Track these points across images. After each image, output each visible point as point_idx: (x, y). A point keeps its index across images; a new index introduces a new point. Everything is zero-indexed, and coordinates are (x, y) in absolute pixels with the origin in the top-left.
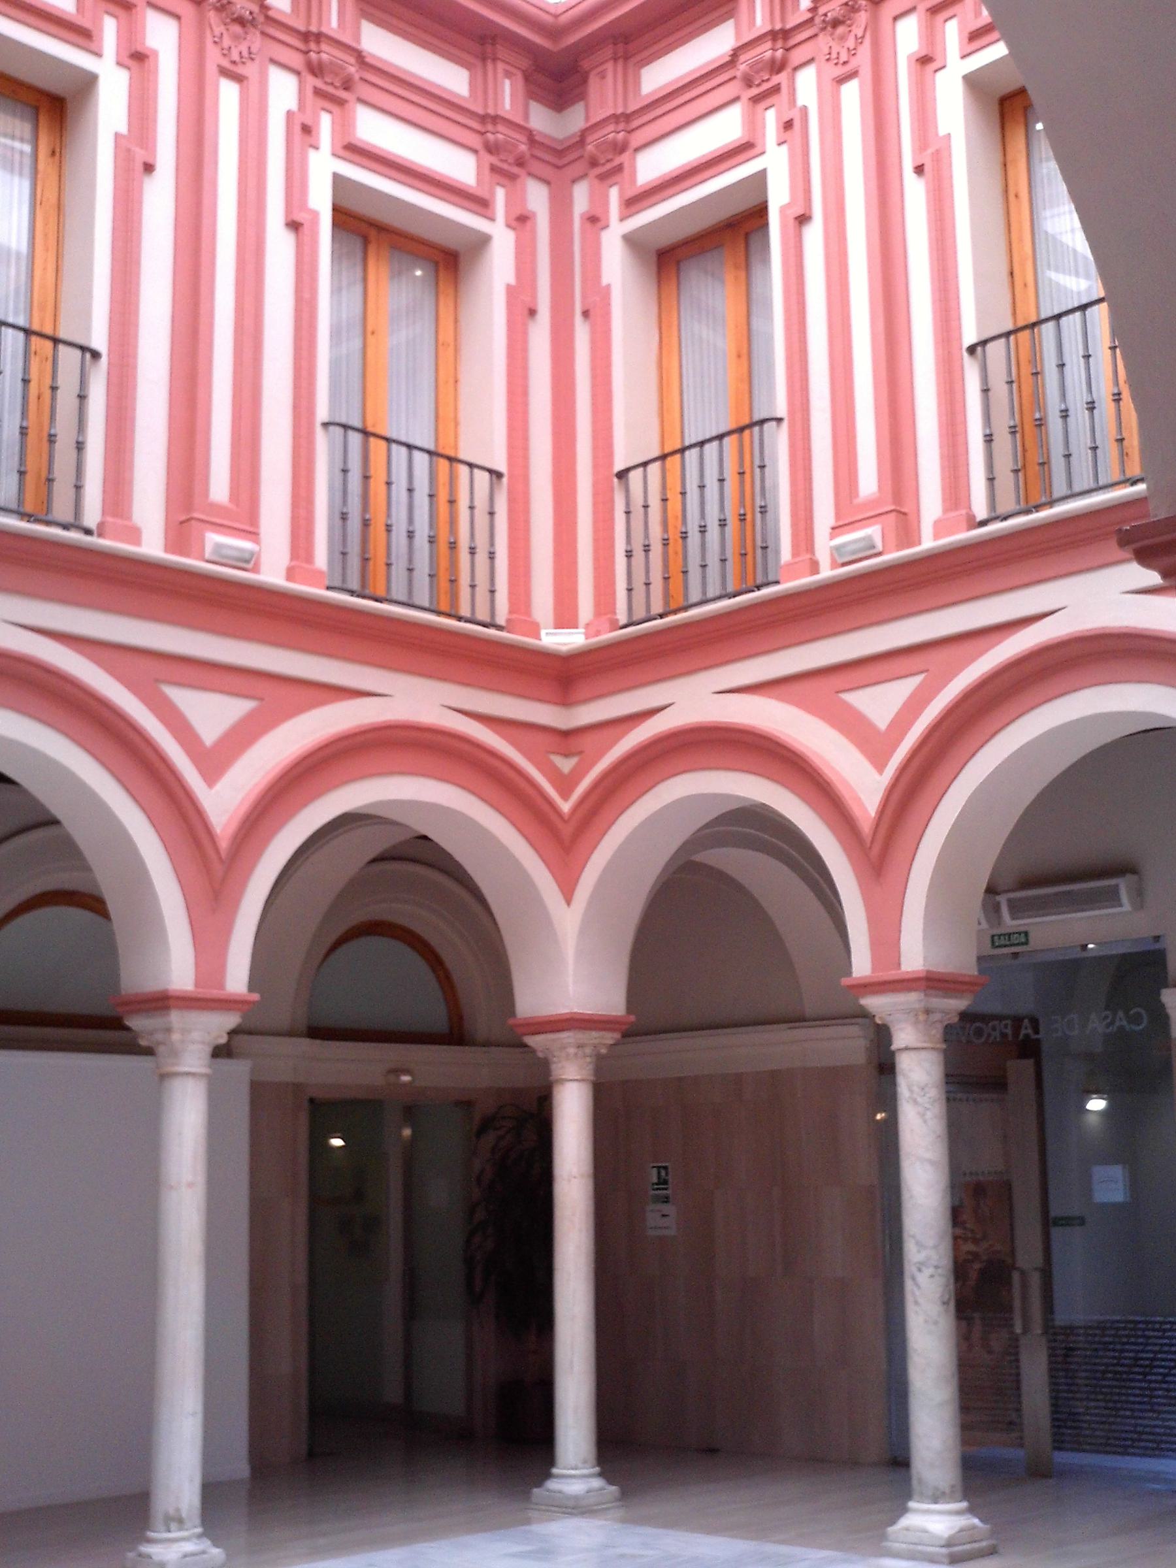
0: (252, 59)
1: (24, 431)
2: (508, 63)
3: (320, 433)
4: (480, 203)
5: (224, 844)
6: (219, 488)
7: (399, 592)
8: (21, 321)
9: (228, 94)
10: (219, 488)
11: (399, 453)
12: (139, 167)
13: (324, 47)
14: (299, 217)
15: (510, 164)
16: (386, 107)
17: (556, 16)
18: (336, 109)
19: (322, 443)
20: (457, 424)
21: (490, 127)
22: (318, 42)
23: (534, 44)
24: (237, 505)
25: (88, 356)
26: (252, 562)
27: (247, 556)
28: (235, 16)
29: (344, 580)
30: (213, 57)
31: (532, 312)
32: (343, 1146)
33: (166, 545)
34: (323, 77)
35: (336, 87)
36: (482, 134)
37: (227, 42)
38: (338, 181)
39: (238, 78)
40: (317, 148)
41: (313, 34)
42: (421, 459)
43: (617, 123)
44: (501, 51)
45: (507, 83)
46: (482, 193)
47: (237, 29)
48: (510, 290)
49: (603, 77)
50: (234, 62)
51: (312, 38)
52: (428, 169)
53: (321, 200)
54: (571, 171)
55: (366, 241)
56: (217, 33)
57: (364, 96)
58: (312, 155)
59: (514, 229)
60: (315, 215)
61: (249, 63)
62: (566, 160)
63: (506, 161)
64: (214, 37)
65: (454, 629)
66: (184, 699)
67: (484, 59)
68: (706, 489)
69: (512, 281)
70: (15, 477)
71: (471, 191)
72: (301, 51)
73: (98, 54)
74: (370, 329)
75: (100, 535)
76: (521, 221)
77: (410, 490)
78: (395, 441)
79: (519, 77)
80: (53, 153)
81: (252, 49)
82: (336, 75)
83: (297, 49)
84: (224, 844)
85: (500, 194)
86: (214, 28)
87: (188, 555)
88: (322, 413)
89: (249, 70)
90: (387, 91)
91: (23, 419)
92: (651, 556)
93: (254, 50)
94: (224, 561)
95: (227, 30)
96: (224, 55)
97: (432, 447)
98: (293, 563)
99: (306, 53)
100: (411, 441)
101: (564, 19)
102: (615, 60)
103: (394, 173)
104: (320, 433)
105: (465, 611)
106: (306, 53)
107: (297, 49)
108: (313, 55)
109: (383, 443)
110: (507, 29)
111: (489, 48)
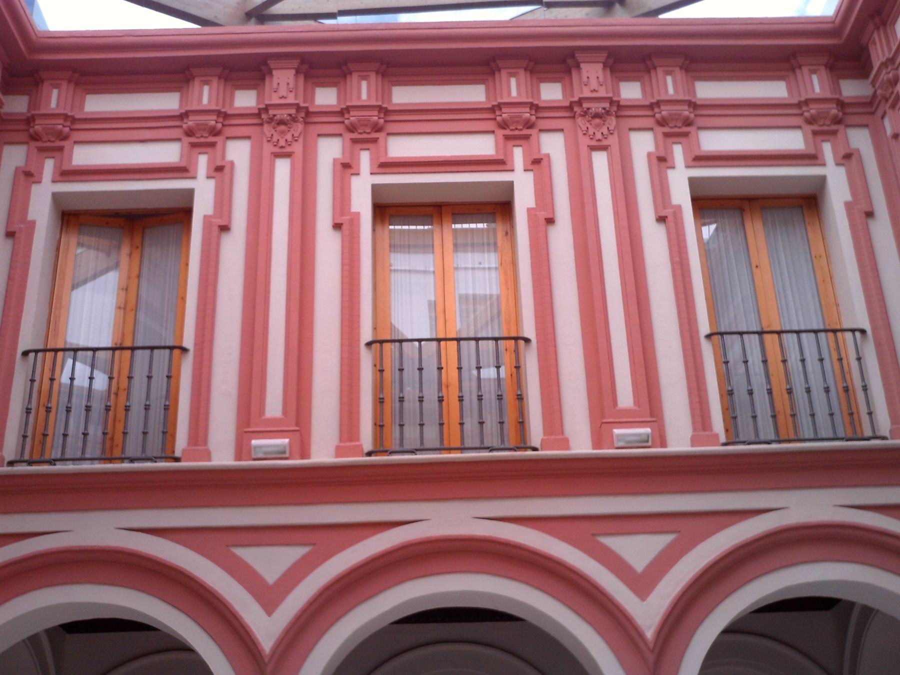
0: (611, 134)
1: (69, 409)
2: (809, 65)
3: (363, 351)
4: (811, 158)
5: (649, 634)
6: (625, 397)
7: (808, 433)
8: (755, 328)
9: (600, 162)
10: (625, 397)
11: (790, 340)
12: (543, 222)
13: (811, 106)
14: (15, 227)
15: (828, 125)
16: (437, 130)
17: (833, 22)
18: (683, 140)
19: (707, 351)
20: (837, 305)
21: (804, 108)
22: (659, 107)
23: (829, 45)
24: (639, 406)
25: (858, 334)
26: (650, 440)
27: (645, 438)
28: (593, 114)
29: (835, 432)
30: (584, 142)
31: (870, 214)
32: (717, 229)
33: (593, 445)
34: (668, 124)
35: (680, 127)
36: (802, 115)
37: (591, 132)
38: (693, 182)
39: (604, 148)
40: (673, 167)
41: (575, 102)
42: (487, 347)
43: (887, 67)
44: (500, 63)
45: (815, 78)
46: (812, 151)
47: (597, 121)
48: (848, 206)
49: (875, 44)
50: (599, 140)
51: (345, 112)
52: (760, 151)
53: (681, 196)
54: (879, 113)
55: (742, 210)
56: (584, 128)
57: (701, 125)
58: (671, 174)
59: (843, 165)
60: (678, 209)
61: (610, 137)
62: (875, 106)
63: (824, 125)
64: (583, 131)
65: (51, 472)
66: (615, 543)
67: (649, 71)
68: (404, 403)
69: (849, 198)
70: (437, 428)
71: (804, 153)
72: (569, 117)
73: (824, 165)
74: (754, 265)
75: (542, 450)
76: (847, 158)
77: (460, 369)
78: (783, 332)
79: (823, 70)
80: (507, 234)
81: (610, 129)
82: (677, 120)
83: (565, 117)
84: (649, 634)
85: (827, 149)
86: (582, 126)
87: (603, 449)
88: (704, 328)
89: (297, 148)
90: (713, 116)
91: (147, 400)
92: (424, 430)
93: (611, 128)
94: (630, 445)
95: (591, 124)
96: (591, 139)
97: (759, 329)
98: (546, 438)
99: (654, 116)
100: (740, 329)
101: (837, 22)
102: (878, 28)
103: (730, 163)
104: (363, 351)
105: (868, 432)
106: (802, 115)
107: (565, 117)
108: (657, 116)
109: (736, 338)
110: (798, 46)
111: (648, 62)
